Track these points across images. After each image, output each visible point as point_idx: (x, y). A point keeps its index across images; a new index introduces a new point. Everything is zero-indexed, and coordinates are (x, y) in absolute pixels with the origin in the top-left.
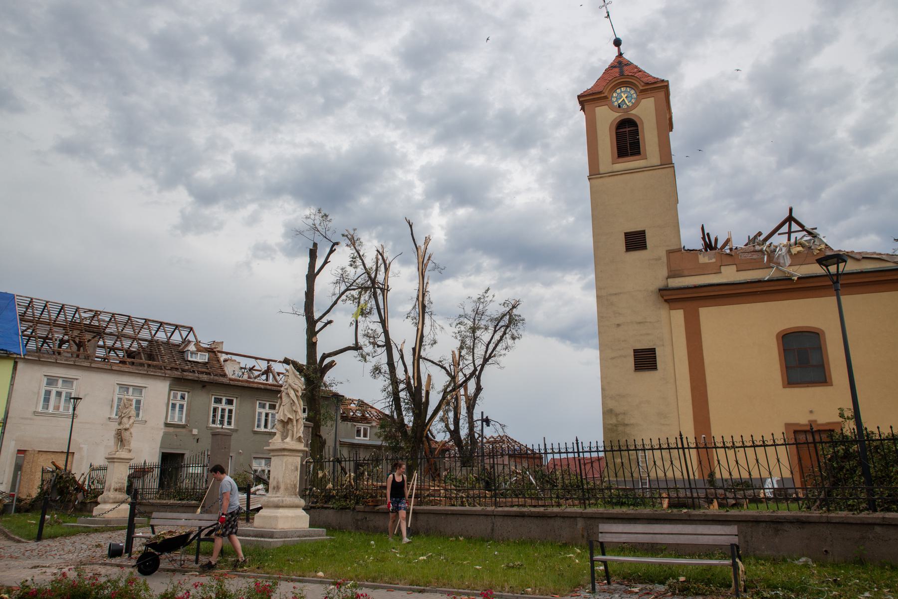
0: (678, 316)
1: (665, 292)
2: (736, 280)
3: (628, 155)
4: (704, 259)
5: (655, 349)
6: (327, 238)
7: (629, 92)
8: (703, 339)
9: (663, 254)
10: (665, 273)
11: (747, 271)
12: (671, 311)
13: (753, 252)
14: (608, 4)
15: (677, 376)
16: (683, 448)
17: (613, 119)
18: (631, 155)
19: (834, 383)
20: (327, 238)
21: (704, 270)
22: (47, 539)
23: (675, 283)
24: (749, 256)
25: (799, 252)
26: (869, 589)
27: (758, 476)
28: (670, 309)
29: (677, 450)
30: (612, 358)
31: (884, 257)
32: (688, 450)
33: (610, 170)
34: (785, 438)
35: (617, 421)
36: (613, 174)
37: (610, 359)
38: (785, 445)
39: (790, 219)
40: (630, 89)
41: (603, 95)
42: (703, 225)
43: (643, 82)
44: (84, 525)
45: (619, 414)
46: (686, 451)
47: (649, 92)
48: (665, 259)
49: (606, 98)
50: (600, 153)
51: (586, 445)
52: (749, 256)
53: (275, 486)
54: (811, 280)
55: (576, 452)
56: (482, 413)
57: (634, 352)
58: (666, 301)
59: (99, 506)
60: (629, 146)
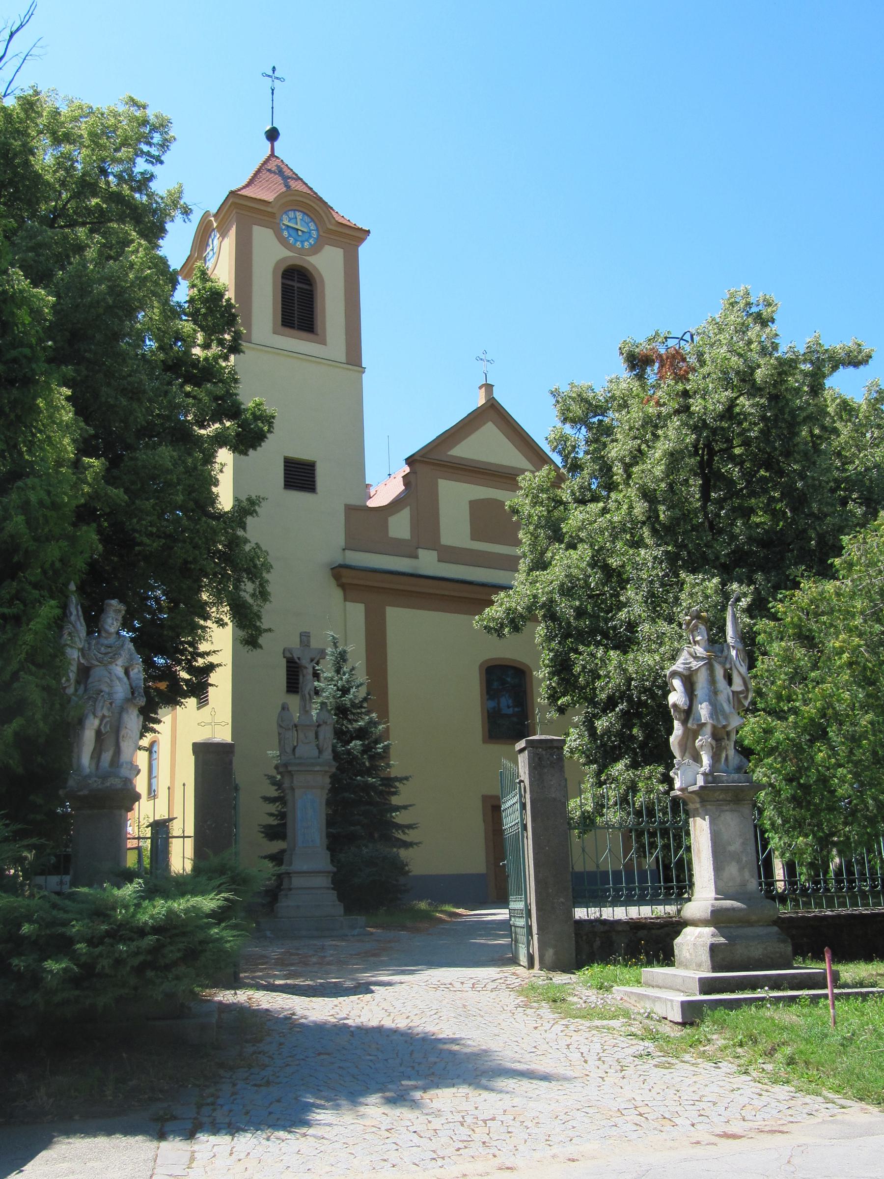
0: (357, 612)
12: (347, 603)
41: (269, 210)
58: (342, 586)
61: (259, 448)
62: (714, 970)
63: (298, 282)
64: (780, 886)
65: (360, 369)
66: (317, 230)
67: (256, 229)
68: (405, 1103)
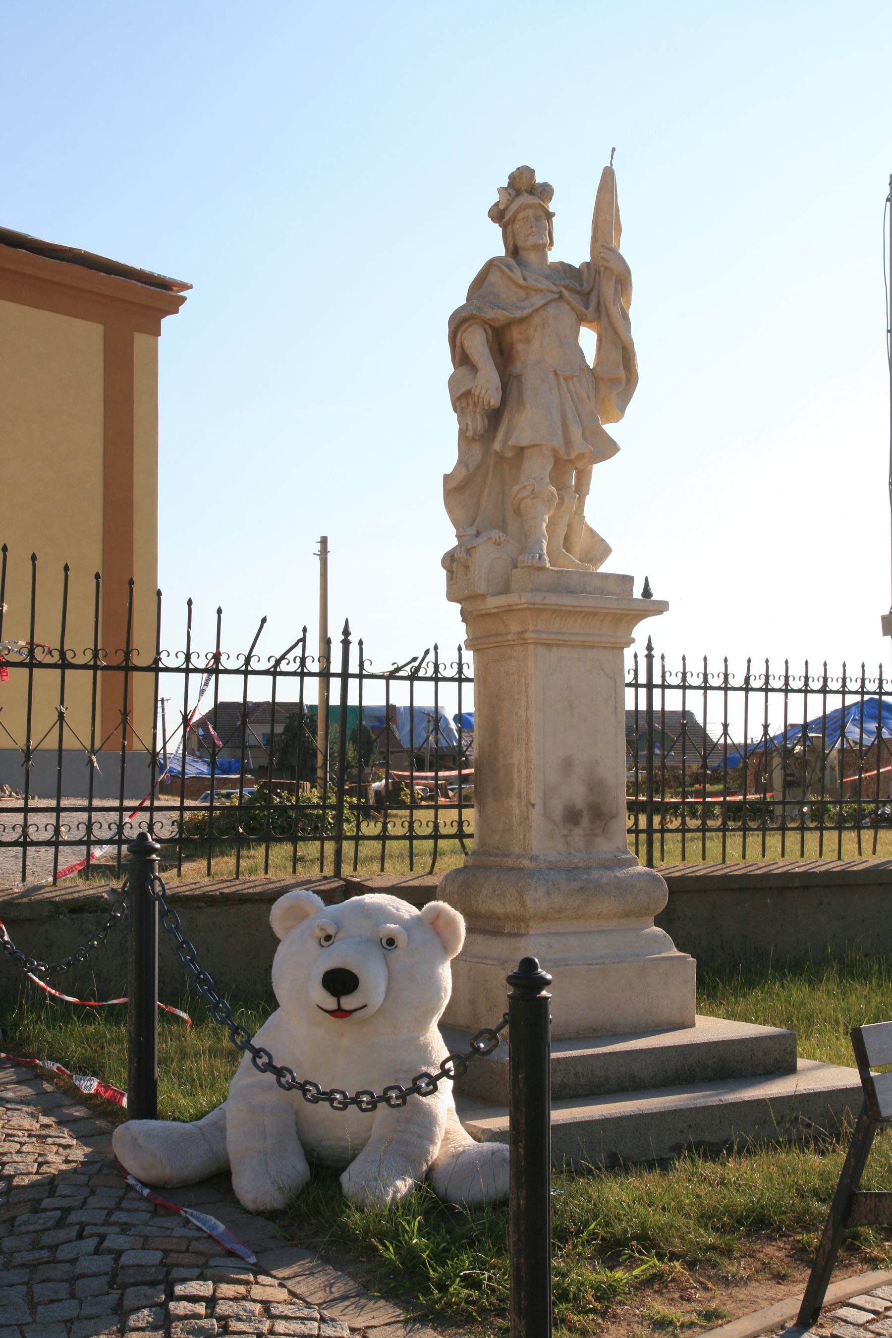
16: (650, 686)
22: (307, 1184)
26: (473, 1211)
29: (457, 684)
32: (660, 690)
34: (99, 647)
38: (95, 668)
51: (674, 666)
53: (580, 804)
55: (642, 686)
56: (314, 554)
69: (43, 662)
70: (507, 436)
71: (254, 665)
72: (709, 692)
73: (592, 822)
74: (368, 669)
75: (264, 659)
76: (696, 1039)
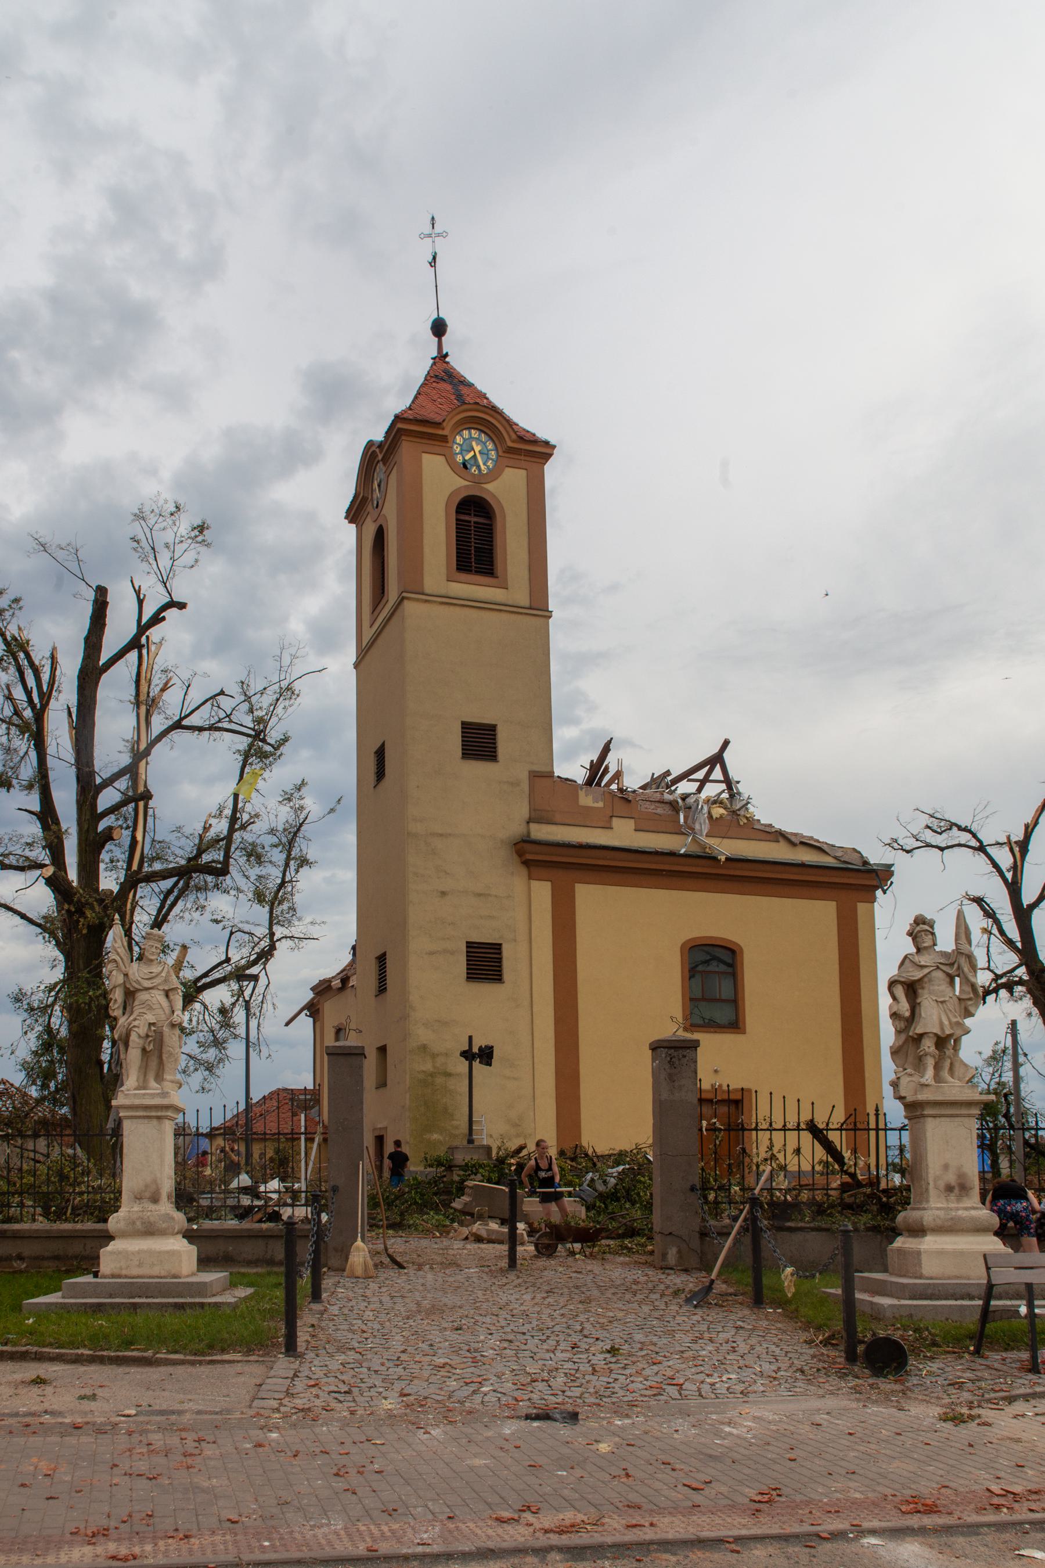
0: (542, 891)
1: (528, 847)
2: (632, 845)
3: (471, 571)
4: (586, 799)
5: (500, 945)
6: (166, 587)
7: (485, 443)
8: (578, 939)
9: (524, 776)
10: (523, 811)
11: (582, 828)
12: (532, 881)
13: (659, 802)
14: (439, 235)
15: (535, 996)
17: (454, 488)
18: (476, 572)
19: (748, 1030)
20: (166, 587)
21: (584, 818)
23: (542, 832)
24: (651, 808)
25: (721, 816)
27: (796, 1168)
28: (530, 878)
30: (431, 953)
31: (825, 847)
33: (443, 592)
35: (434, 1067)
36: (449, 601)
37: (426, 954)
39: (717, 759)
40: (487, 438)
41: (440, 432)
42: (612, 739)
43: (515, 433)
44: (171, 1300)
45: (438, 1055)
46: (882, 1133)
47: (522, 457)
48: (525, 786)
49: (444, 439)
50: (427, 550)
52: (651, 808)
54: (740, 865)
56: (470, 1038)
57: (467, 947)
58: (526, 863)
59: (112, 1246)
60: (473, 552)
61: (347, 521)
62: (685, 1029)
63: (475, 515)
64: (199, 984)
65: (546, 614)
66: (497, 449)
67: (426, 457)
68: (523, 433)
69: (997, 915)
70: (915, 1029)
71: (831, 1126)
72: (857, 1132)
73: (960, 1191)
74: (889, 1126)
75: (835, 1123)
76: (49, 739)
